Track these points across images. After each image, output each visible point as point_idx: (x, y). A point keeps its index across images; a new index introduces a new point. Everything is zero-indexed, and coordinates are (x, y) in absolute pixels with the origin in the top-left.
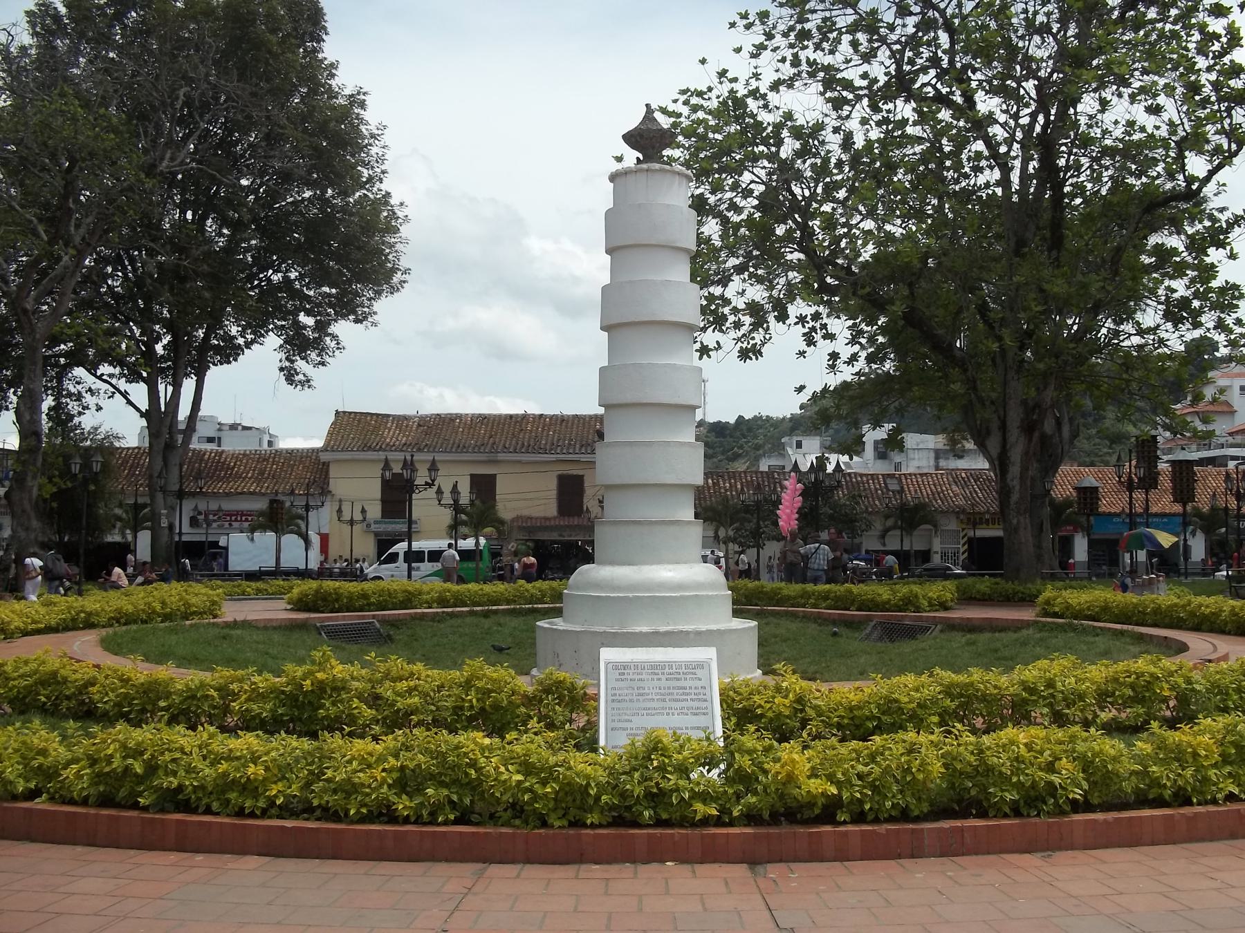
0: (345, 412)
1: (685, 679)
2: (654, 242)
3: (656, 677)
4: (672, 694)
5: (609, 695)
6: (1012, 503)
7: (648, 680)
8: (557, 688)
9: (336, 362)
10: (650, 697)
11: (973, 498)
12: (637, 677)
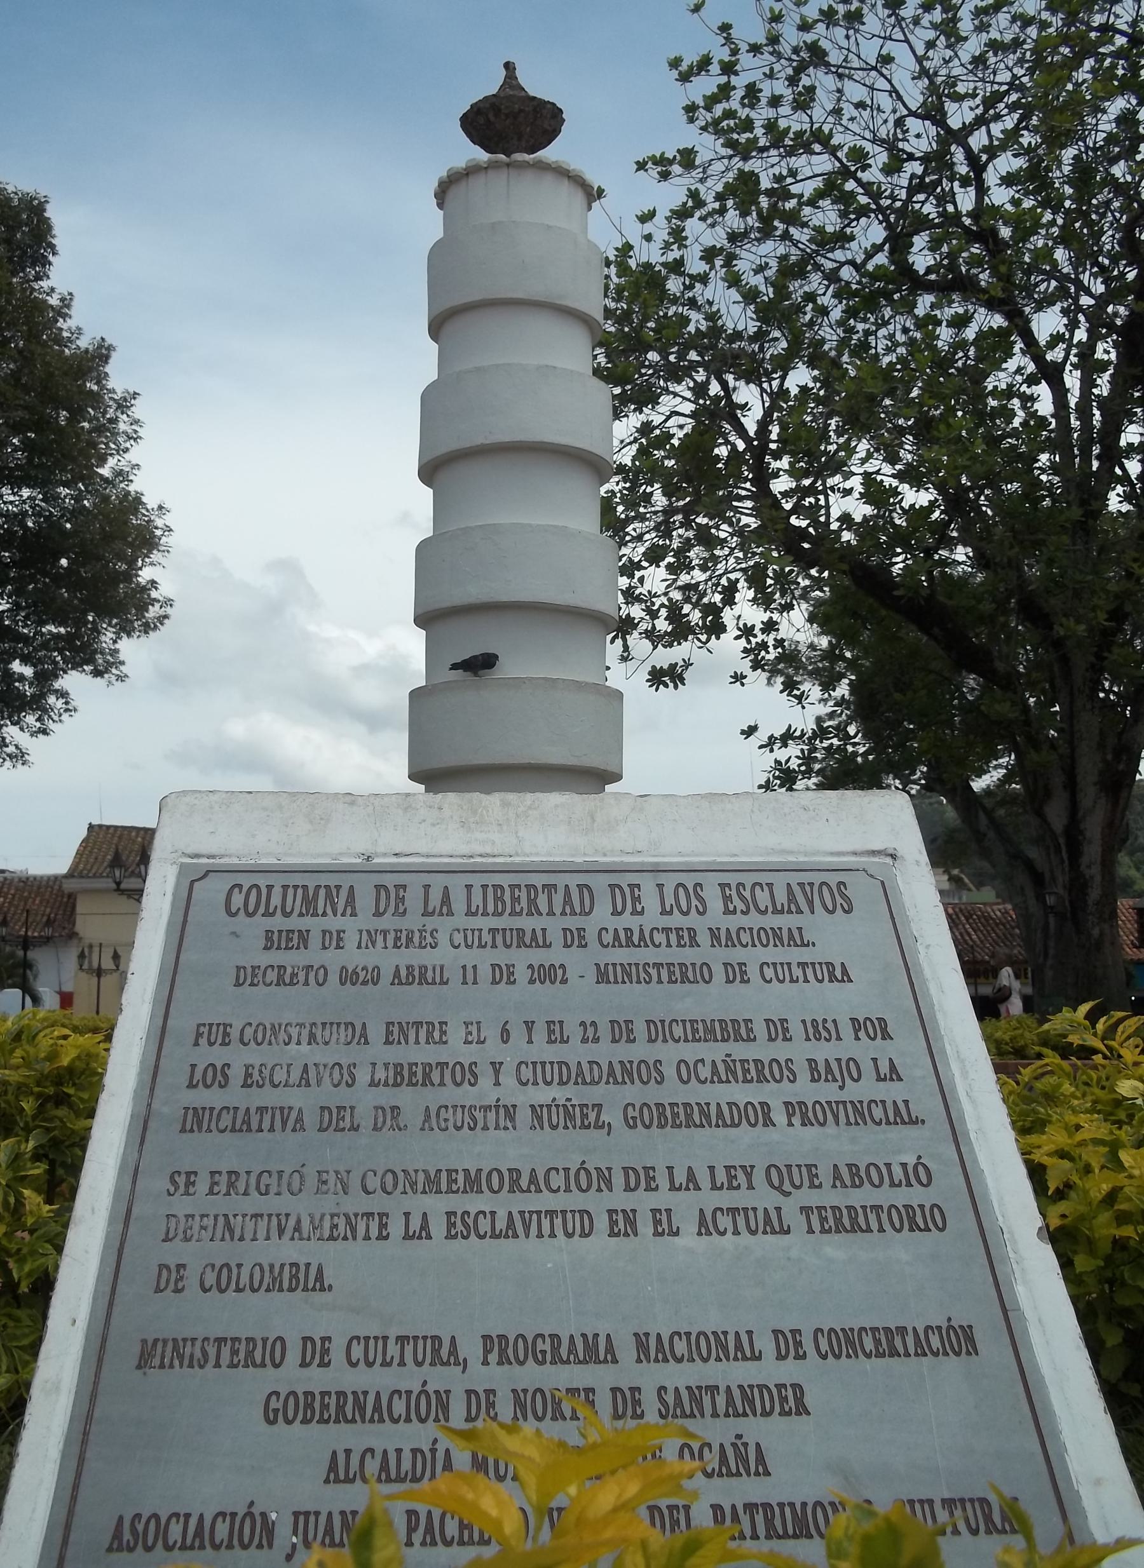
0: (100, 826)
1: (737, 974)
2: (520, 295)
3: (522, 959)
4: (653, 1072)
5: (175, 1072)
6: (1090, 902)
7: (470, 976)
8: (44, 1101)
9: (63, 729)
10: (485, 1091)
11: (965, 941)
12: (388, 960)
